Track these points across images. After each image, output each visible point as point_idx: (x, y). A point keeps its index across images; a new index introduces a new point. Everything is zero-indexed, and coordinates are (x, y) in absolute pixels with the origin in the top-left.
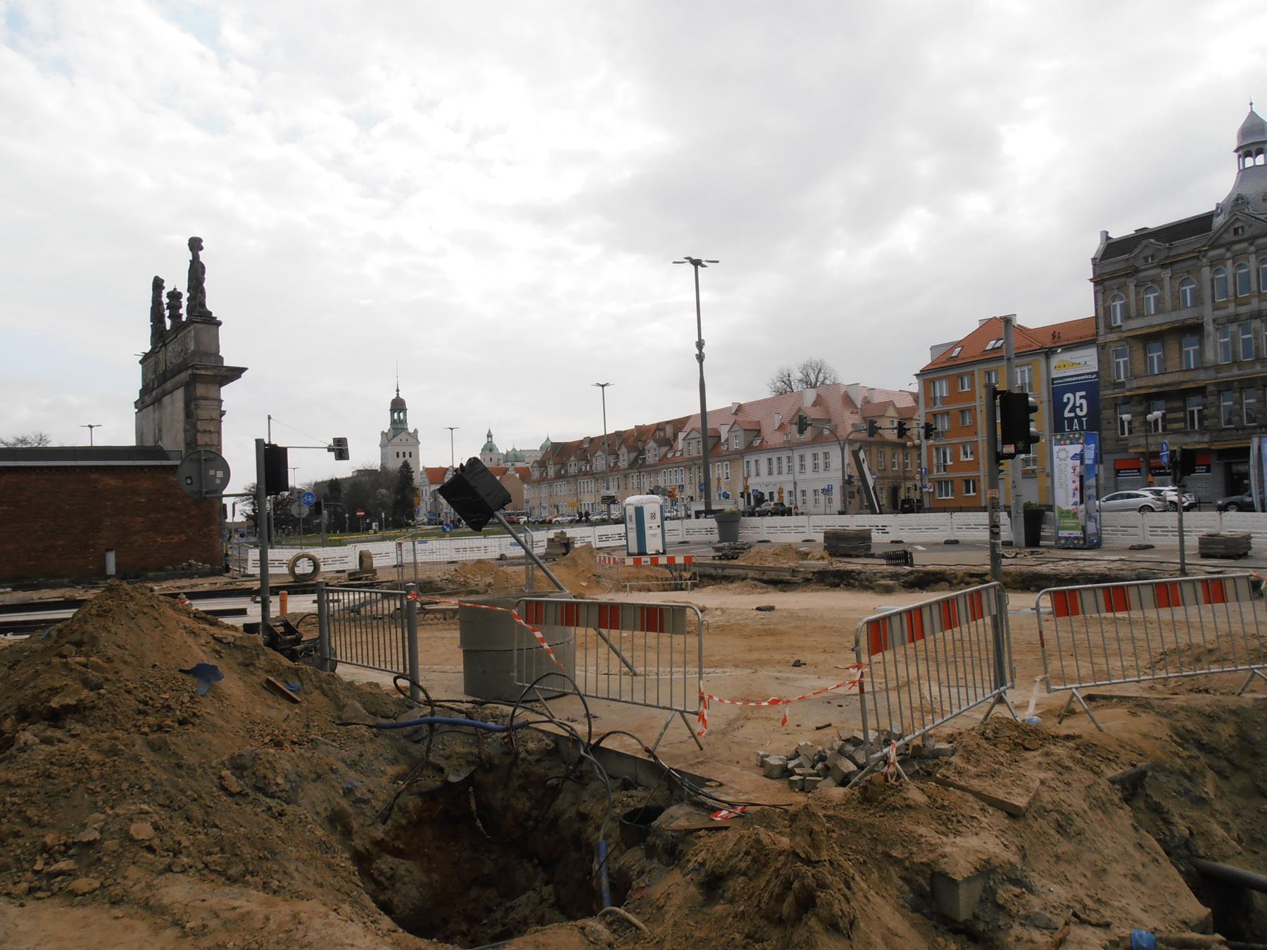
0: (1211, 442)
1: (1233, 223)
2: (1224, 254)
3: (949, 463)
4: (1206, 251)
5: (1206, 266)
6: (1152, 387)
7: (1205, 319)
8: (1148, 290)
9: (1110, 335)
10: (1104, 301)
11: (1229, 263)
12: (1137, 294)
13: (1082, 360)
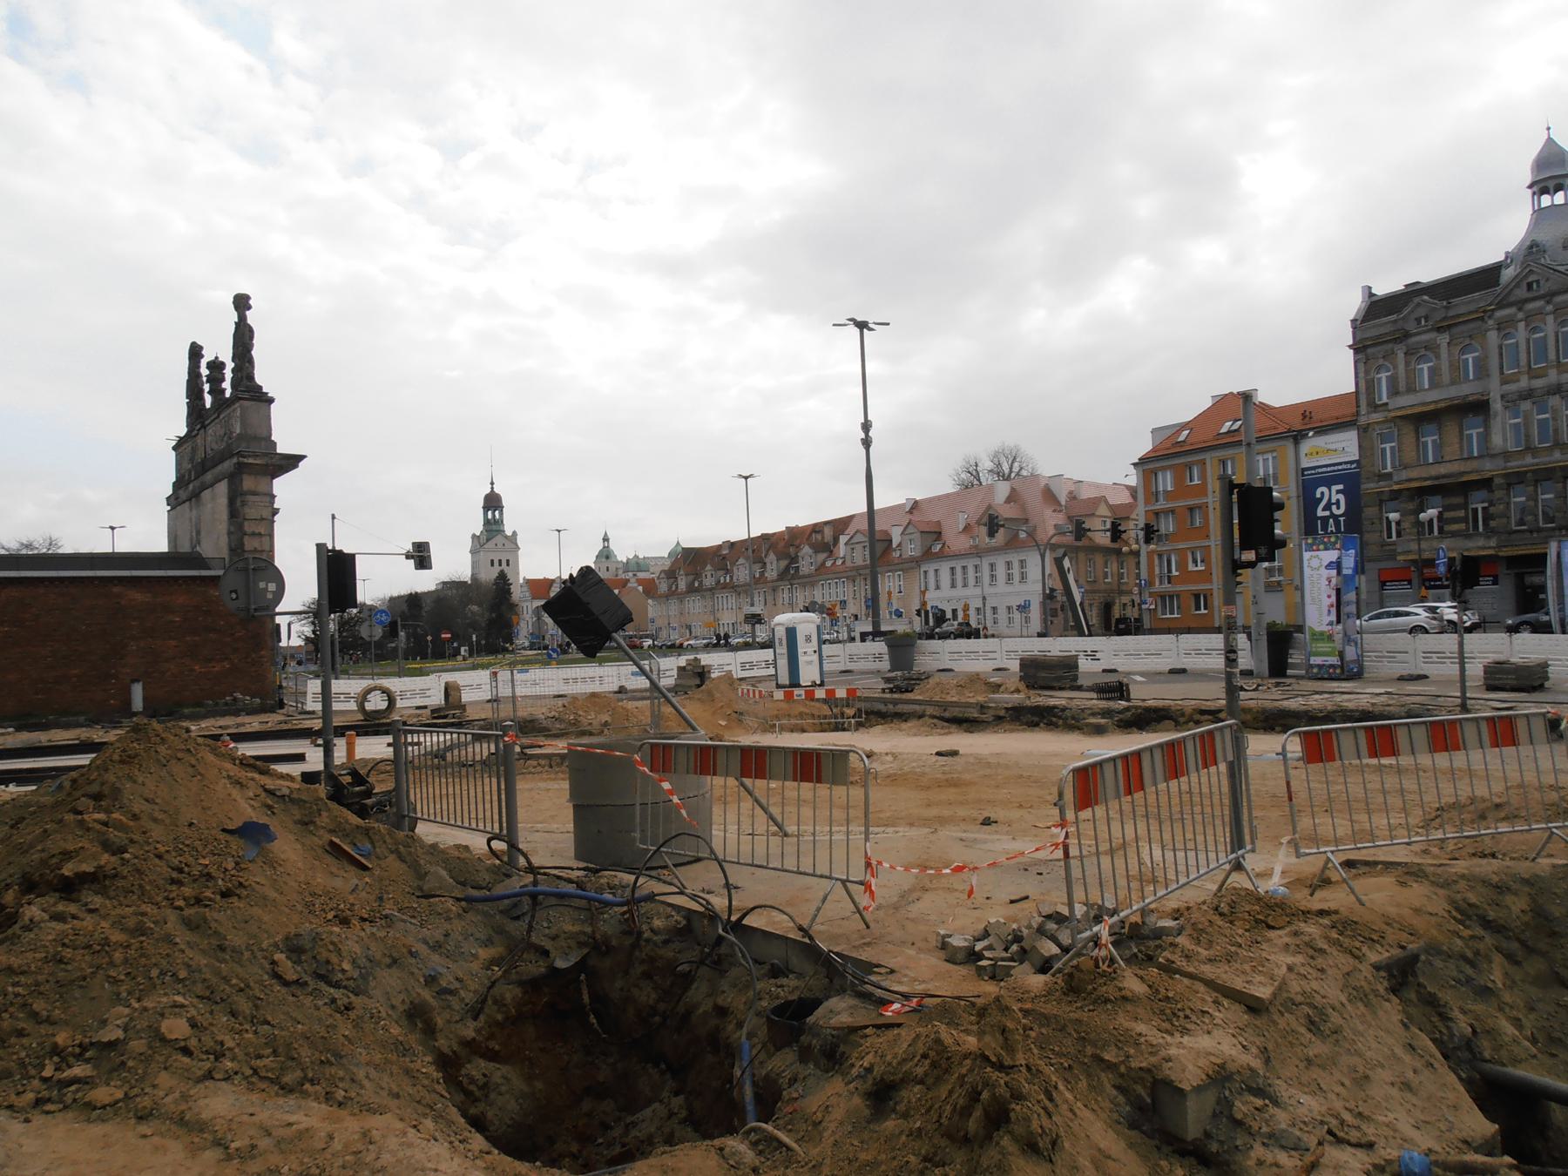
0: (1499, 547)
1: (1526, 276)
2: (1515, 315)
3: (1175, 573)
4: (1493, 310)
5: (1492, 329)
6: (1426, 479)
7: (1491, 395)
8: (1421, 359)
9: (1374, 415)
10: (1367, 372)
11: (1522, 325)
12: (1407, 364)
13: (1339, 446)
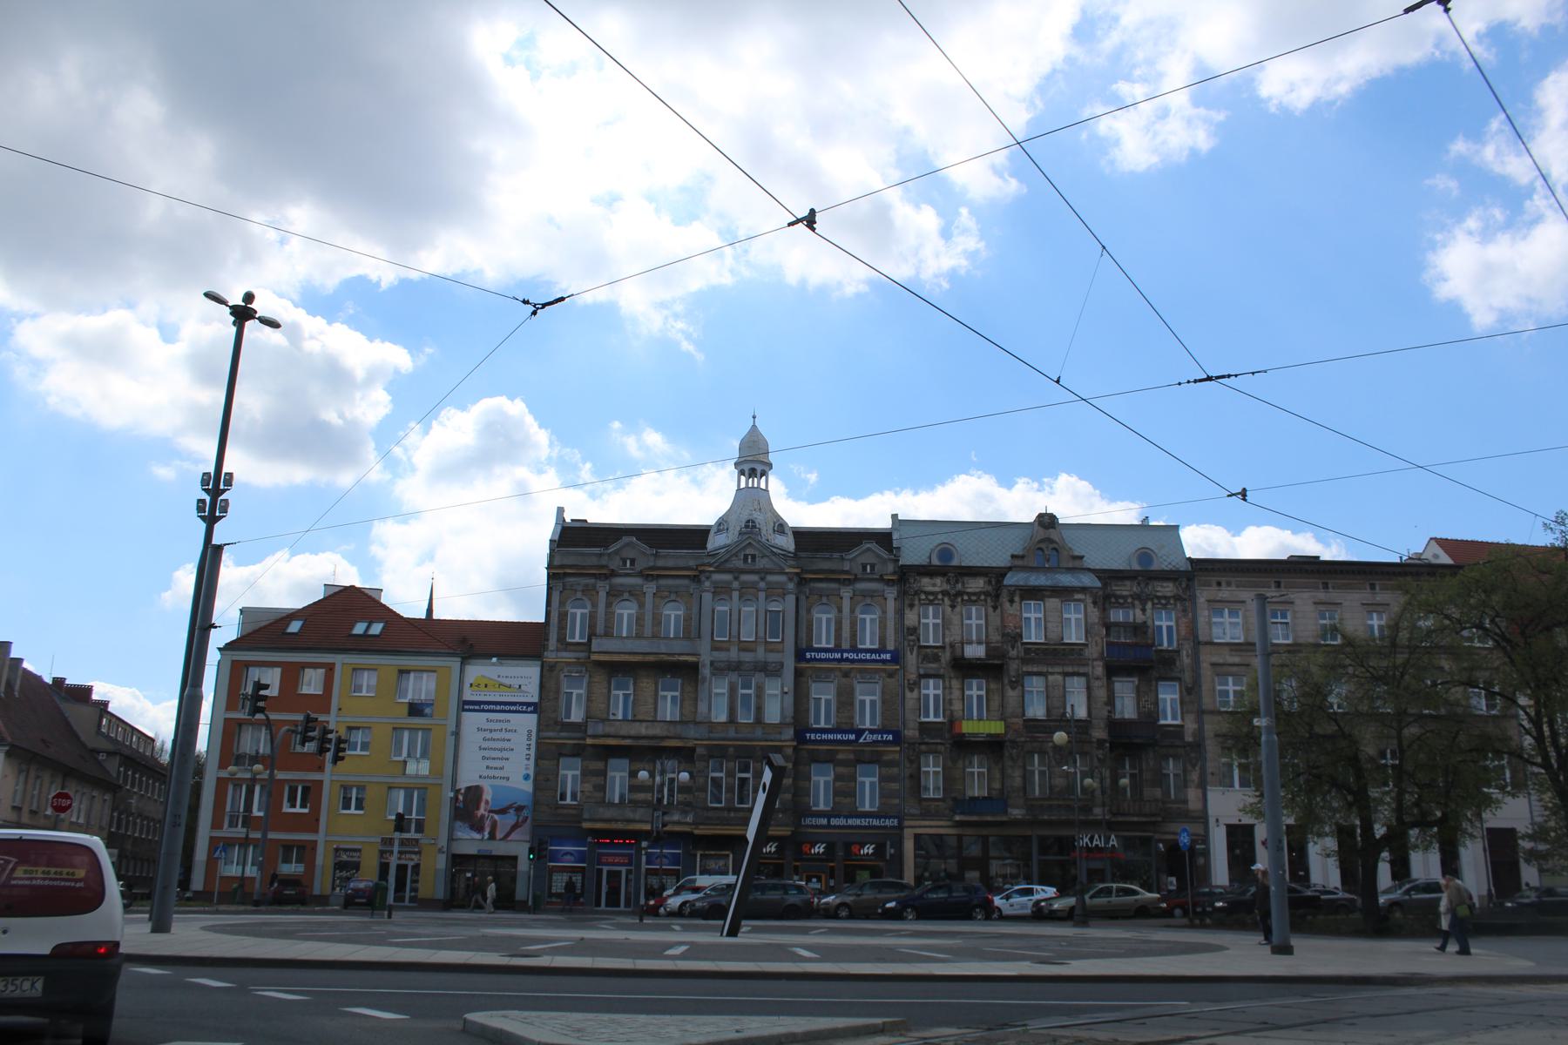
0: (695, 824)
1: (744, 548)
2: (731, 583)
3: (256, 812)
5: (708, 591)
8: (867, 609)
9: (564, 654)
10: (562, 603)
12: (609, 605)
13: (515, 683)
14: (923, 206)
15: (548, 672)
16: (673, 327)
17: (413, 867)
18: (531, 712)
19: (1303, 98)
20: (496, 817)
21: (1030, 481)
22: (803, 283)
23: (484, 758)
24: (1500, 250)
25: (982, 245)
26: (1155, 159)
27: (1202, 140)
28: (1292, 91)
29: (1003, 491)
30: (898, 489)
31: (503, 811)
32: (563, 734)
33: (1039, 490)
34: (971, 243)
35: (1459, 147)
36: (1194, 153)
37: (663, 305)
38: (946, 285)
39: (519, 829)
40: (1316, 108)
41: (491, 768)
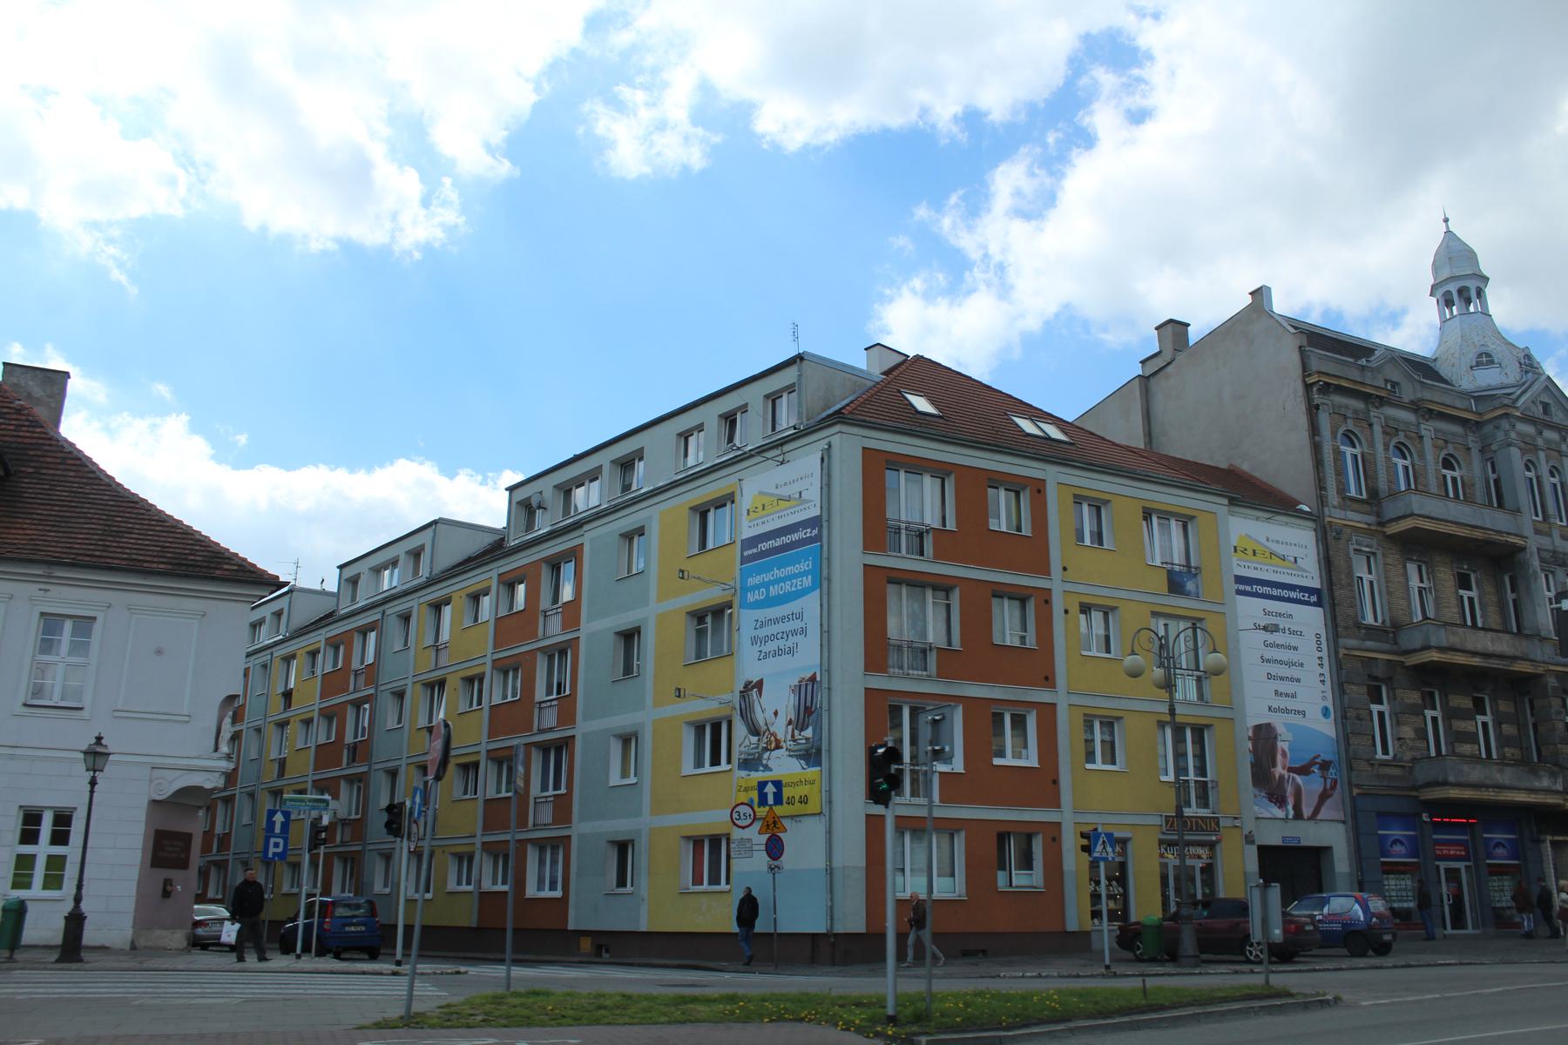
14: (407, 168)
15: (1328, 538)
16: (103, 251)
17: (1202, 870)
18: (1314, 604)
19: (794, 141)
20: (1299, 779)
21: (474, 474)
22: (264, 228)
23: (1270, 676)
24: (941, 312)
25: (461, 220)
26: (647, 170)
27: (696, 158)
28: (784, 132)
29: (445, 480)
30: (333, 466)
31: (1304, 770)
32: (1369, 644)
33: (481, 484)
34: (451, 216)
35: (922, 212)
36: (686, 169)
37: (95, 226)
38: (417, 255)
39: (1329, 801)
40: (807, 150)
41: (1281, 694)
